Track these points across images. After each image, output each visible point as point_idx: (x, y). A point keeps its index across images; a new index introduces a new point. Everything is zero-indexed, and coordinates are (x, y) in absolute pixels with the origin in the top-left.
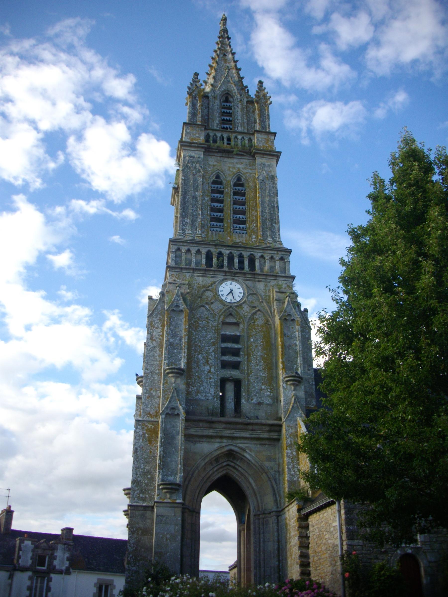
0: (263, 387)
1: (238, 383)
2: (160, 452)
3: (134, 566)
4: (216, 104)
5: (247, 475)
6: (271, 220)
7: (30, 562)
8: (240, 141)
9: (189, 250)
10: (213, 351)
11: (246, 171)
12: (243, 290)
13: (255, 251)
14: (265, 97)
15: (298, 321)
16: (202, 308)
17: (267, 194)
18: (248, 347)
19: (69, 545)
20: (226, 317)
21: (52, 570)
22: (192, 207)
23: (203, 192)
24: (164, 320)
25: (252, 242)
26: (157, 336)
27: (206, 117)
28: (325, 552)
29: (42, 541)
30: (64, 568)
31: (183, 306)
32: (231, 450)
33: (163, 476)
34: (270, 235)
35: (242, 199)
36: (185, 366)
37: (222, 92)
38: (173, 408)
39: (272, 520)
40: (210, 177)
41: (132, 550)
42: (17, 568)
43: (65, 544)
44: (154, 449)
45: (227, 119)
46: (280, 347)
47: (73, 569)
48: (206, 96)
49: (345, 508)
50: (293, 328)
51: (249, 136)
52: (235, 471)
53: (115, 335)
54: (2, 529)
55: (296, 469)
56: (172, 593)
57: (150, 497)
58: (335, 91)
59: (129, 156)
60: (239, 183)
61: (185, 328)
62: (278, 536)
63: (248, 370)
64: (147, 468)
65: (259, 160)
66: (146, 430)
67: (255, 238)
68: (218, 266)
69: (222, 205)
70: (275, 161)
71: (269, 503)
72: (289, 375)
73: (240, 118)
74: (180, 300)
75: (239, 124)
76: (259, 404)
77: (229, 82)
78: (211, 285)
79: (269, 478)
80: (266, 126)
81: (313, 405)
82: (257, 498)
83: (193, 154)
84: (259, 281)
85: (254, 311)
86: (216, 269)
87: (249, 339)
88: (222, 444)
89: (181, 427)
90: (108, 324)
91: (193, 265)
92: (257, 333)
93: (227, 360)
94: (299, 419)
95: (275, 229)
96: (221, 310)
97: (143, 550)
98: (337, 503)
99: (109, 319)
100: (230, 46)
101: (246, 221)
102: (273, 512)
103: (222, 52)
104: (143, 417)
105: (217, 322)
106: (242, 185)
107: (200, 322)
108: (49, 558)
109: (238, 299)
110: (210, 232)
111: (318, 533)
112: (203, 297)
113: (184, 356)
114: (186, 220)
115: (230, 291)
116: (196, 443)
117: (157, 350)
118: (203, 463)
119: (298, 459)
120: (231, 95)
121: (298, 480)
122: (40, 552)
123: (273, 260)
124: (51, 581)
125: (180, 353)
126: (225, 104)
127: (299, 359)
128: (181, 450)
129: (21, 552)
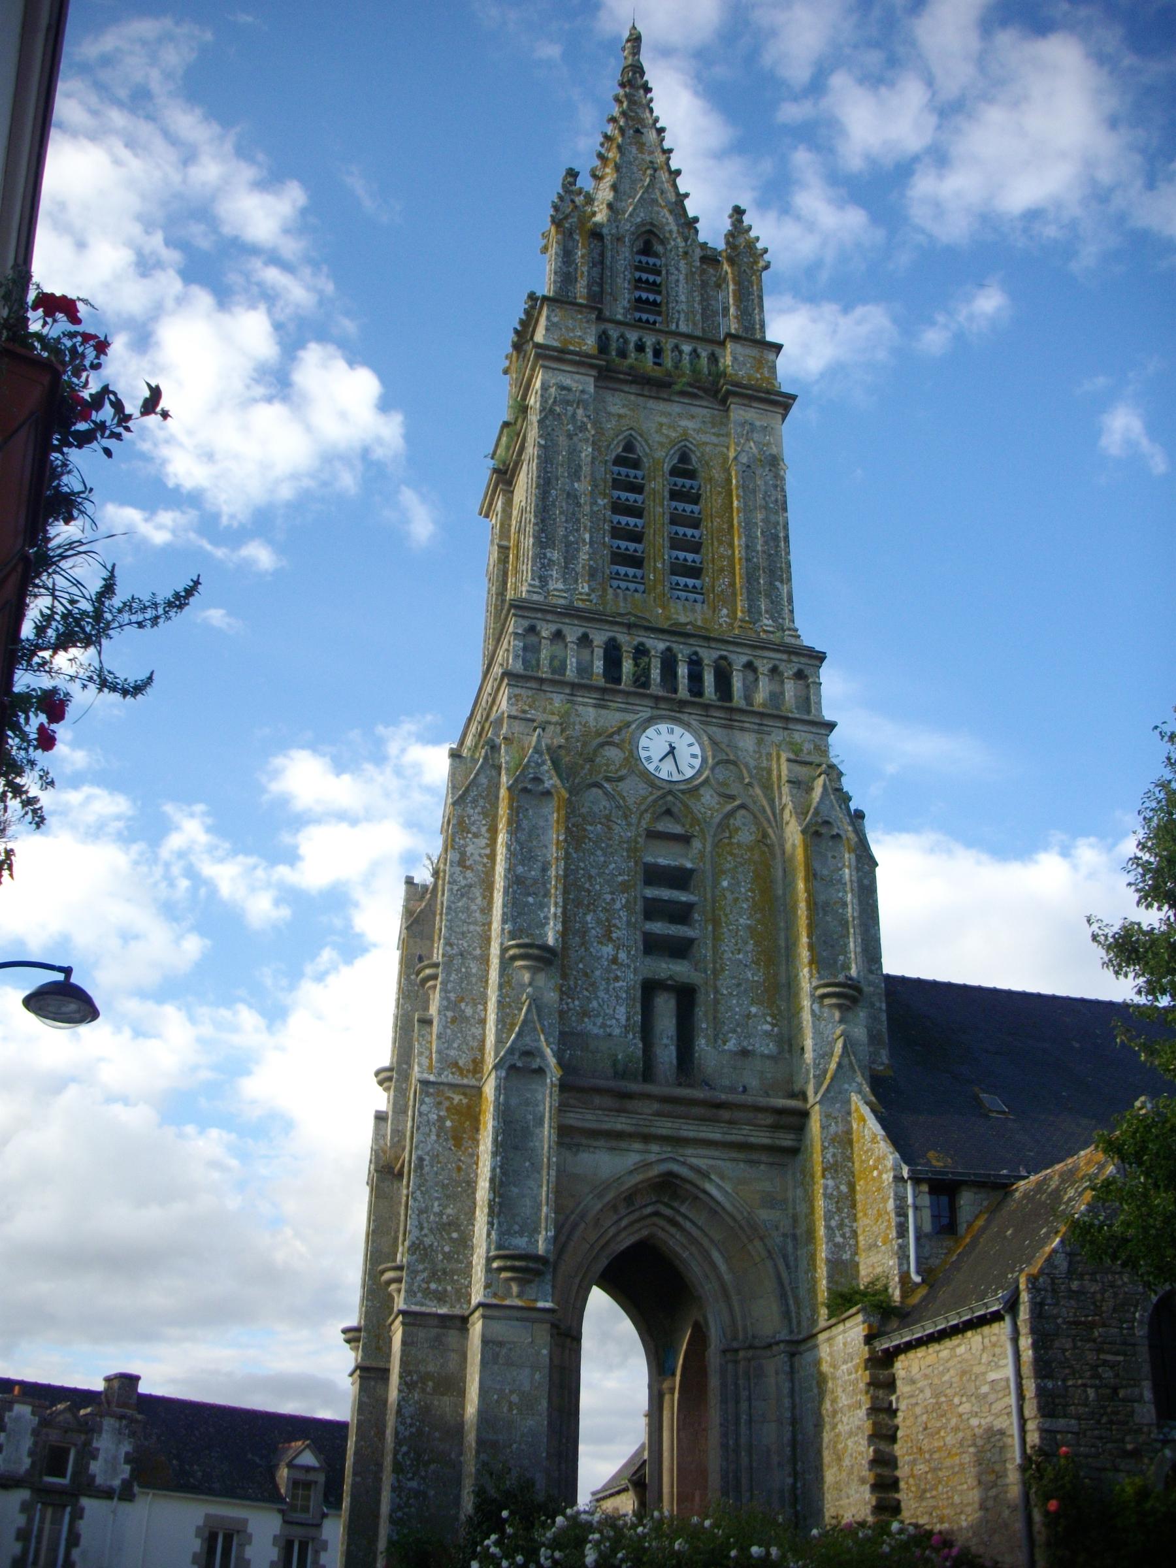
0: (754, 1010)
1: (686, 996)
2: (493, 1170)
3: (412, 1479)
5: (705, 1242)
6: (771, 570)
7: (27, 1462)
8: (686, 359)
9: (558, 635)
10: (624, 906)
11: (704, 438)
12: (702, 750)
13: (731, 648)
14: (751, 248)
15: (848, 839)
16: (594, 790)
17: (760, 502)
18: (714, 902)
19: (132, 1420)
20: (657, 818)
21: (85, 1486)
22: (566, 521)
25: (721, 625)
26: (478, 858)
28: (954, 1450)
29: (60, 1407)
30: (117, 1483)
31: (551, 781)
32: (670, 1174)
33: (501, 1234)
34: (767, 612)
35: (692, 512)
36: (557, 940)
37: (638, 226)
38: (528, 1054)
39: (774, 1365)
40: (609, 446)
43: (122, 1417)
44: (469, 1161)
45: (648, 299)
46: (802, 905)
47: (140, 1486)
48: (596, 234)
49: (1033, 1331)
50: (834, 857)
51: (710, 348)
52: (673, 1230)
53: (191, 873)
55: (847, 1229)
57: (458, 1291)
58: (824, 276)
59: (269, 400)
60: (684, 467)
61: (558, 840)
63: (715, 962)
64: (449, 1211)
65: (738, 413)
66: (448, 1109)
67: (728, 616)
68: (635, 682)
69: (639, 522)
71: (767, 1318)
72: (826, 981)
73: (683, 298)
74: (544, 763)
75: (682, 315)
76: (745, 1053)
77: (654, 202)
78: (620, 730)
79: (769, 1252)
80: (754, 324)
81: (883, 1064)
83: (567, 381)
84: (742, 729)
85: (729, 807)
86: (632, 689)
87: (716, 884)
88: (647, 1156)
89: (547, 1105)
90: (175, 841)
91: (570, 674)
92: (736, 867)
94: (855, 1098)
95: (779, 596)
96: (645, 798)
98: (1008, 1318)
99: (178, 828)
100: (651, 111)
101: (701, 569)
102: (777, 1343)
103: (631, 123)
104: (440, 1075)
105: (633, 828)
106: (691, 474)
107: (589, 828)
108: (78, 1453)
109: (689, 773)
110: (610, 591)
111: (934, 1401)
113: (555, 914)
114: (549, 555)
115: (668, 749)
116: (578, 1150)
117: (478, 894)
118: (599, 1206)
119: (853, 1206)
120: (658, 237)
121: (852, 1260)
122: (54, 1436)
123: (777, 678)
124: (81, 1517)
125: (542, 906)
126: (644, 259)
127: (851, 940)
128: (549, 1168)
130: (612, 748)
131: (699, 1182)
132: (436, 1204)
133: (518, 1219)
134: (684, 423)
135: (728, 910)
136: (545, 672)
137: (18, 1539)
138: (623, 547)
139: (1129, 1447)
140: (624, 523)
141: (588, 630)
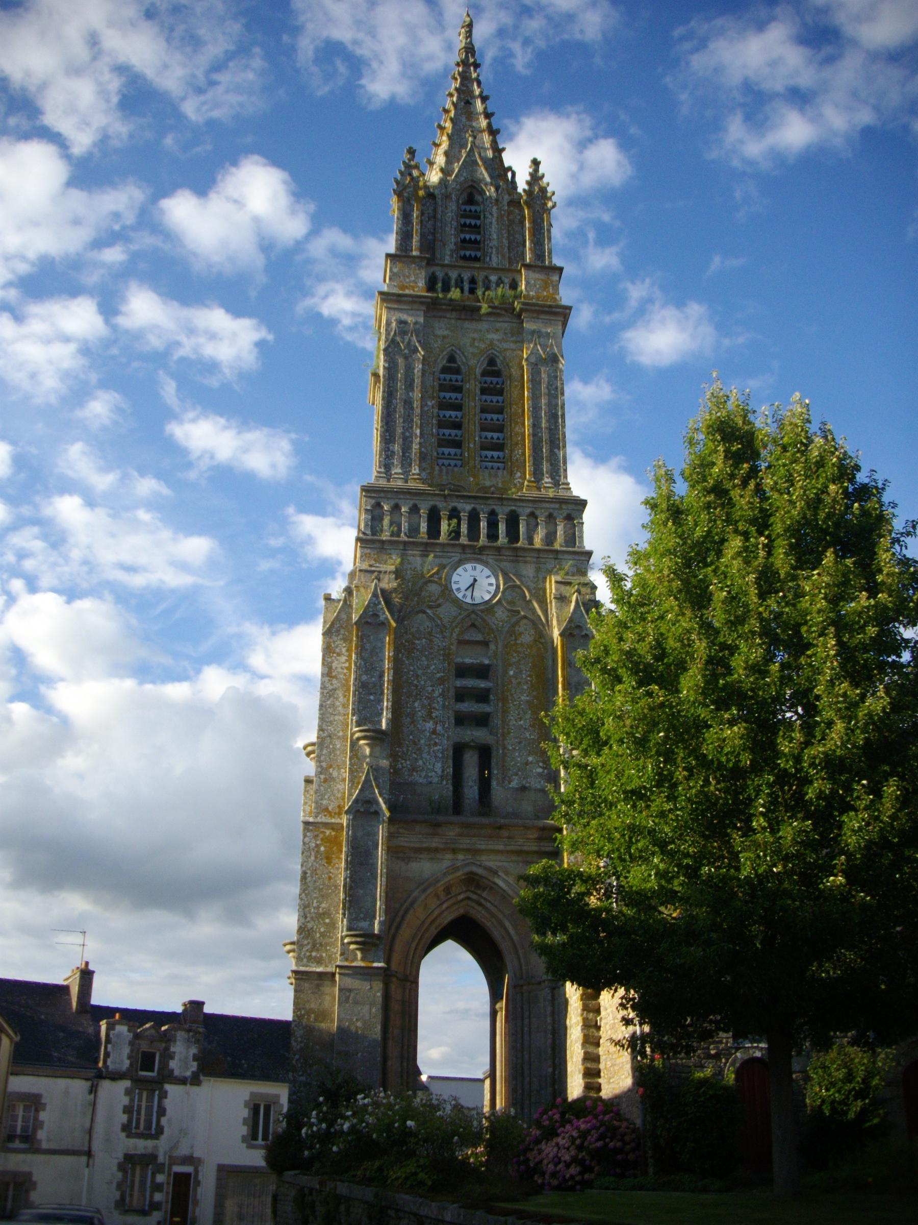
0: (530, 759)
1: (485, 754)
2: (345, 879)
3: (302, 1075)
4: (449, 210)
5: (500, 916)
7: (127, 1063)
10: (440, 694)
11: (506, 346)
16: (420, 615)
19: (197, 1033)
21: (167, 1076)
23: (424, 391)
24: (351, 641)
26: (340, 670)
27: (430, 237)
29: (147, 1026)
30: (188, 1074)
33: (349, 921)
35: (498, 402)
40: (436, 361)
42: (104, 1074)
43: (189, 1031)
47: (205, 1076)
52: (480, 909)
54: (74, 1004)
56: (355, 1121)
66: (322, 840)
67: (520, 477)
69: (459, 414)
70: (560, 323)
73: (495, 236)
75: (494, 250)
76: (523, 789)
83: (404, 317)
84: (525, 562)
85: (514, 619)
87: (506, 672)
95: (558, 460)
96: (456, 617)
101: (504, 444)
102: (544, 981)
103: (462, 96)
104: (316, 817)
106: (498, 374)
107: (417, 642)
108: (161, 1056)
112: (423, 594)
114: (391, 448)
122: (145, 1047)
126: (468, 208)
129: (109, 1046)
131: (491, 878)
133: (363, 910)
136: (385, 536)
137: (124, 1112)
139: (713, 1052)
140: (447, 416)
141: (417, 502)
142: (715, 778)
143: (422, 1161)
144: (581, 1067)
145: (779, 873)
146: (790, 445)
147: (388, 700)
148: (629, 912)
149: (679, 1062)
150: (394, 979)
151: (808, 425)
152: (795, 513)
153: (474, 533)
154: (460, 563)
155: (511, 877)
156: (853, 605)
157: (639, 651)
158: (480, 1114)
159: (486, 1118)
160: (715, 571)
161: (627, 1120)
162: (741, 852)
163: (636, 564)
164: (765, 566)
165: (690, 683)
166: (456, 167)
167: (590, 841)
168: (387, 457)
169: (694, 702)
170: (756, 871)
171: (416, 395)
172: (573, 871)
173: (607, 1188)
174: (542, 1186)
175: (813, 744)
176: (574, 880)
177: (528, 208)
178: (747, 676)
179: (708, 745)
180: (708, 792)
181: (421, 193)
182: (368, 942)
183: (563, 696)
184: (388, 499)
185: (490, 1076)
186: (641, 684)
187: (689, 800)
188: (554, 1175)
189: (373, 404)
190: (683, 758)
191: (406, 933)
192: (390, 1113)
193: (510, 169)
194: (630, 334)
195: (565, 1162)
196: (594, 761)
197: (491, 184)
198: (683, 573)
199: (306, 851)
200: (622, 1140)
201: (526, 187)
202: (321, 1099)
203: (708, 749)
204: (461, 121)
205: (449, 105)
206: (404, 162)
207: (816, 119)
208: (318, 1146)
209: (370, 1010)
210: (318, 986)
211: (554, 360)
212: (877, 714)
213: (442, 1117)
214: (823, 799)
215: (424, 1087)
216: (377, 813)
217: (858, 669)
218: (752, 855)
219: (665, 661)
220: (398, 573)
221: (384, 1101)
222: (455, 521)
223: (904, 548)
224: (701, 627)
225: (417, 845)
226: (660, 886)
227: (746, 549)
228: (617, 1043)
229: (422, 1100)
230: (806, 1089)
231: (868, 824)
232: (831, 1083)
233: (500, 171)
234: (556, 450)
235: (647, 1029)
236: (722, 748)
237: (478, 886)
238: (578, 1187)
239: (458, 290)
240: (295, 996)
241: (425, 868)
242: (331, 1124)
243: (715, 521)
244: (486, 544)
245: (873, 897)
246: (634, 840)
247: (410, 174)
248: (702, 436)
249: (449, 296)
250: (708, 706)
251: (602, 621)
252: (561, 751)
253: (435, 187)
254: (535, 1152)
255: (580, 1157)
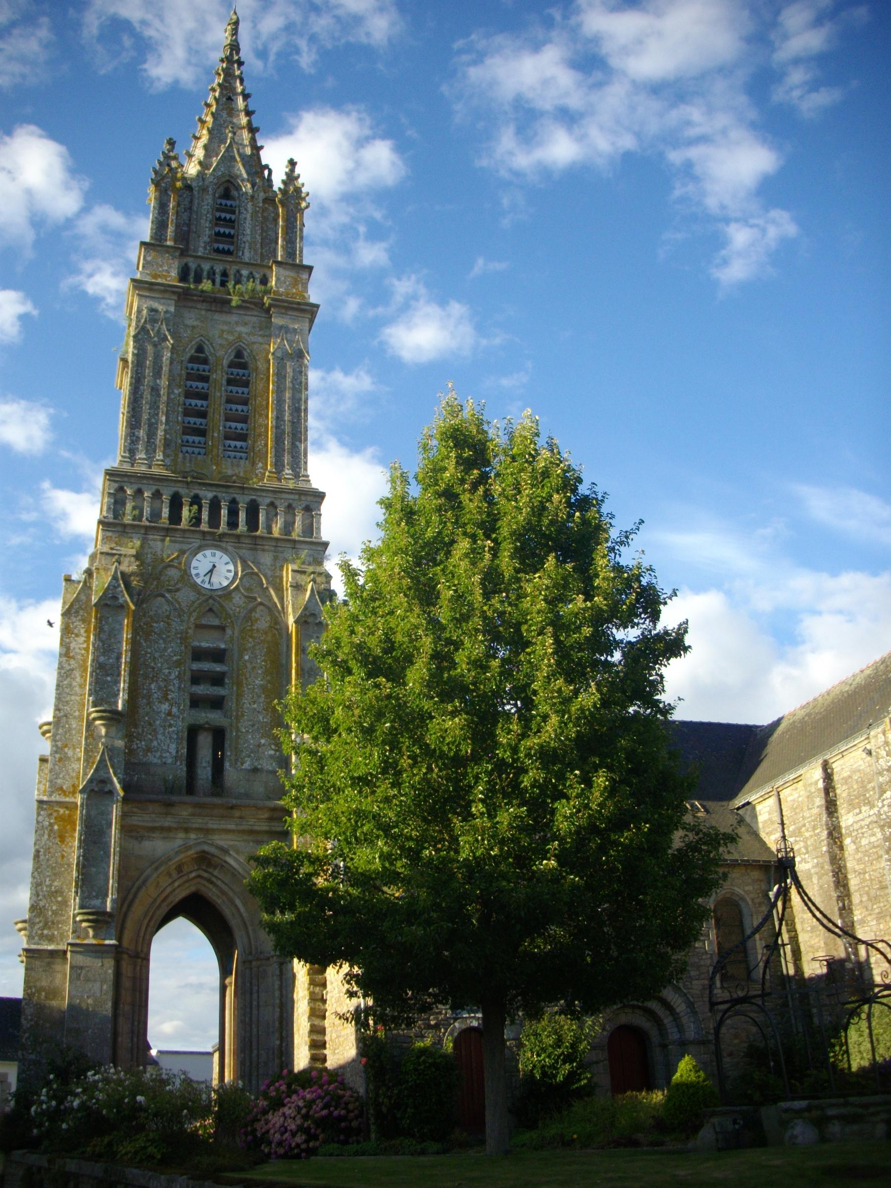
0: (263, 741)
1: (219, 736)
2: (78, 858)
3: (32, 1053)
4: (205, 203)
5: (231, 894)
11: (253, 339)
13: (259, 494)
16: (159, 598)
23: (171, 380)
24: (90, 622)
32: (204, 852)
33: (81, 899)
35: (243, 393)
40: (184, 350)
41: (29, 1025)
45: (224, 232)
52: (211, 886)
56: (85, 1098)
60: (240, 361)
62: (281, 995)
66: (56, 818)
67: (262, 468)
69: (205, 403)
73: (248, 231)
75: (247, 244)
76: (255, 770)
82: (247, 932)
83: (156, 305)
84: (263, 550)
85: (251, 605)
87: (241, 656)
93: (200, 692)
96: (194, 602)
97: (48, 1025)
101: (247, 434)
102: (272, 957)
103: (225, 92)
104: (51, 796)
106: (244, 366)
107: (155, 625)
114: (136, 433)
120: (234, 185)
126: (224, 202)
130: (172, 569)
132: (48, 879)
134: (239, 329)
135: (248, 676)
136: (128, 519)
138: (192, 422)
139: (432, 1023)
140: (193, 404)
142: (437, 766)
143: (151, 1136)
144: (307, 1039)
145: (496, 855)
146: (519, 455)
147: (124, 681)
148: (355, 892)
149: (401, 1032)
150: (125, 956)
151: (536, 438)
152: (521, 518)
153: (214, 520)
154: (200, 549)
155: (242, 856)
156: (570, 606)
157: (369, 645)
158: (209, 1088)
159: (214, 1091)
160: (443, 570)
161: (351, 1089)
162: (460, 836)
163: (369, 560)
164: (490, 568)
165: (417, 674)
166: (215, 161)
167: (318, 825)
168: (132, 442)
169: (419, 695)
170: (474, 854)
171: (164, 382)
172: (301, 853)
173: (331, 1155)
174: (269, 1155)
175: (529, 736)
176: (302, 862)
177: (283, 206)
178: (469, 670)
179: (431, 735)
180: (431, 779)
181: (179, 184)
182: (100, 920)
183: (296, 685)
184: (131, 483)
185: (219, 1049)
186: (370, 675)
187: (413, 787)
188: (280, 1144)
189: (120, 388)
190: (408, 747)
191: (138, 910)
192: (120, 1089)
193: (267, 167)
194: (388, 331)
195: (291, 1131)
196: (323, 747)
197: (248, 181)
198: (413, 571)
199: (39, 829)
200: (346, 1108)
201: (282, 186)
202: (52, 1076)
203: (431, 739)
204: (222, 117)
205: (211, 100)
206: (163, 152)
207: (581, 139)
208: (47, 1124)
209: (102, 986)
210: (49, 964)
211: (299, 355)
212: (589, 709)
213: (171, 1092)
214: (537, 787)
215: (154, 1062)
216: (111, 793)
217: (573, 667)
218: (471, 839)
219: (394, 654)
220: (137, 557)
221: (115, 1077)
222: (196, 507)
223: (617, 556)
224: (428, 623)
225: (150, 824)
226: (384, 867)
227: (473, 551)
228: (342, 1017)
229: (152, 1075)
230: (519, 1055)
231: (579, 811)
232: (542, 1049)
233: (257, 168)
234: (297, 443)
235: (370, 1002)
236: (444, 738)
237: (210, 864)
238: (303, 1155)
239: (209, 281)
240: (26, 974)
241: (158, 846)
242: (60, 1102)
243: (445, 522)
244: (226, 531)
245: (581, 878)
246: (359, 824)
247: (169, 165)
248: (435, 442)
249: (200, 287)
250: (433, 698)
251: (335, 614)
252: (293, 736)
253: (192, 179)
254: (263, 1122)
255: (306, 1125)
